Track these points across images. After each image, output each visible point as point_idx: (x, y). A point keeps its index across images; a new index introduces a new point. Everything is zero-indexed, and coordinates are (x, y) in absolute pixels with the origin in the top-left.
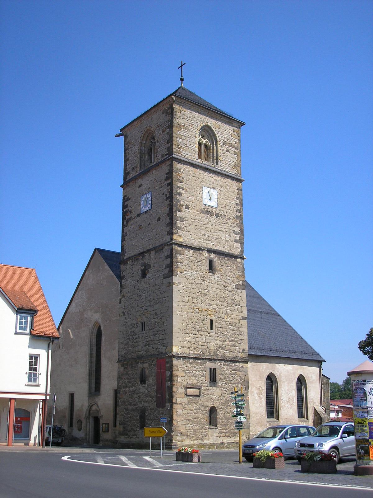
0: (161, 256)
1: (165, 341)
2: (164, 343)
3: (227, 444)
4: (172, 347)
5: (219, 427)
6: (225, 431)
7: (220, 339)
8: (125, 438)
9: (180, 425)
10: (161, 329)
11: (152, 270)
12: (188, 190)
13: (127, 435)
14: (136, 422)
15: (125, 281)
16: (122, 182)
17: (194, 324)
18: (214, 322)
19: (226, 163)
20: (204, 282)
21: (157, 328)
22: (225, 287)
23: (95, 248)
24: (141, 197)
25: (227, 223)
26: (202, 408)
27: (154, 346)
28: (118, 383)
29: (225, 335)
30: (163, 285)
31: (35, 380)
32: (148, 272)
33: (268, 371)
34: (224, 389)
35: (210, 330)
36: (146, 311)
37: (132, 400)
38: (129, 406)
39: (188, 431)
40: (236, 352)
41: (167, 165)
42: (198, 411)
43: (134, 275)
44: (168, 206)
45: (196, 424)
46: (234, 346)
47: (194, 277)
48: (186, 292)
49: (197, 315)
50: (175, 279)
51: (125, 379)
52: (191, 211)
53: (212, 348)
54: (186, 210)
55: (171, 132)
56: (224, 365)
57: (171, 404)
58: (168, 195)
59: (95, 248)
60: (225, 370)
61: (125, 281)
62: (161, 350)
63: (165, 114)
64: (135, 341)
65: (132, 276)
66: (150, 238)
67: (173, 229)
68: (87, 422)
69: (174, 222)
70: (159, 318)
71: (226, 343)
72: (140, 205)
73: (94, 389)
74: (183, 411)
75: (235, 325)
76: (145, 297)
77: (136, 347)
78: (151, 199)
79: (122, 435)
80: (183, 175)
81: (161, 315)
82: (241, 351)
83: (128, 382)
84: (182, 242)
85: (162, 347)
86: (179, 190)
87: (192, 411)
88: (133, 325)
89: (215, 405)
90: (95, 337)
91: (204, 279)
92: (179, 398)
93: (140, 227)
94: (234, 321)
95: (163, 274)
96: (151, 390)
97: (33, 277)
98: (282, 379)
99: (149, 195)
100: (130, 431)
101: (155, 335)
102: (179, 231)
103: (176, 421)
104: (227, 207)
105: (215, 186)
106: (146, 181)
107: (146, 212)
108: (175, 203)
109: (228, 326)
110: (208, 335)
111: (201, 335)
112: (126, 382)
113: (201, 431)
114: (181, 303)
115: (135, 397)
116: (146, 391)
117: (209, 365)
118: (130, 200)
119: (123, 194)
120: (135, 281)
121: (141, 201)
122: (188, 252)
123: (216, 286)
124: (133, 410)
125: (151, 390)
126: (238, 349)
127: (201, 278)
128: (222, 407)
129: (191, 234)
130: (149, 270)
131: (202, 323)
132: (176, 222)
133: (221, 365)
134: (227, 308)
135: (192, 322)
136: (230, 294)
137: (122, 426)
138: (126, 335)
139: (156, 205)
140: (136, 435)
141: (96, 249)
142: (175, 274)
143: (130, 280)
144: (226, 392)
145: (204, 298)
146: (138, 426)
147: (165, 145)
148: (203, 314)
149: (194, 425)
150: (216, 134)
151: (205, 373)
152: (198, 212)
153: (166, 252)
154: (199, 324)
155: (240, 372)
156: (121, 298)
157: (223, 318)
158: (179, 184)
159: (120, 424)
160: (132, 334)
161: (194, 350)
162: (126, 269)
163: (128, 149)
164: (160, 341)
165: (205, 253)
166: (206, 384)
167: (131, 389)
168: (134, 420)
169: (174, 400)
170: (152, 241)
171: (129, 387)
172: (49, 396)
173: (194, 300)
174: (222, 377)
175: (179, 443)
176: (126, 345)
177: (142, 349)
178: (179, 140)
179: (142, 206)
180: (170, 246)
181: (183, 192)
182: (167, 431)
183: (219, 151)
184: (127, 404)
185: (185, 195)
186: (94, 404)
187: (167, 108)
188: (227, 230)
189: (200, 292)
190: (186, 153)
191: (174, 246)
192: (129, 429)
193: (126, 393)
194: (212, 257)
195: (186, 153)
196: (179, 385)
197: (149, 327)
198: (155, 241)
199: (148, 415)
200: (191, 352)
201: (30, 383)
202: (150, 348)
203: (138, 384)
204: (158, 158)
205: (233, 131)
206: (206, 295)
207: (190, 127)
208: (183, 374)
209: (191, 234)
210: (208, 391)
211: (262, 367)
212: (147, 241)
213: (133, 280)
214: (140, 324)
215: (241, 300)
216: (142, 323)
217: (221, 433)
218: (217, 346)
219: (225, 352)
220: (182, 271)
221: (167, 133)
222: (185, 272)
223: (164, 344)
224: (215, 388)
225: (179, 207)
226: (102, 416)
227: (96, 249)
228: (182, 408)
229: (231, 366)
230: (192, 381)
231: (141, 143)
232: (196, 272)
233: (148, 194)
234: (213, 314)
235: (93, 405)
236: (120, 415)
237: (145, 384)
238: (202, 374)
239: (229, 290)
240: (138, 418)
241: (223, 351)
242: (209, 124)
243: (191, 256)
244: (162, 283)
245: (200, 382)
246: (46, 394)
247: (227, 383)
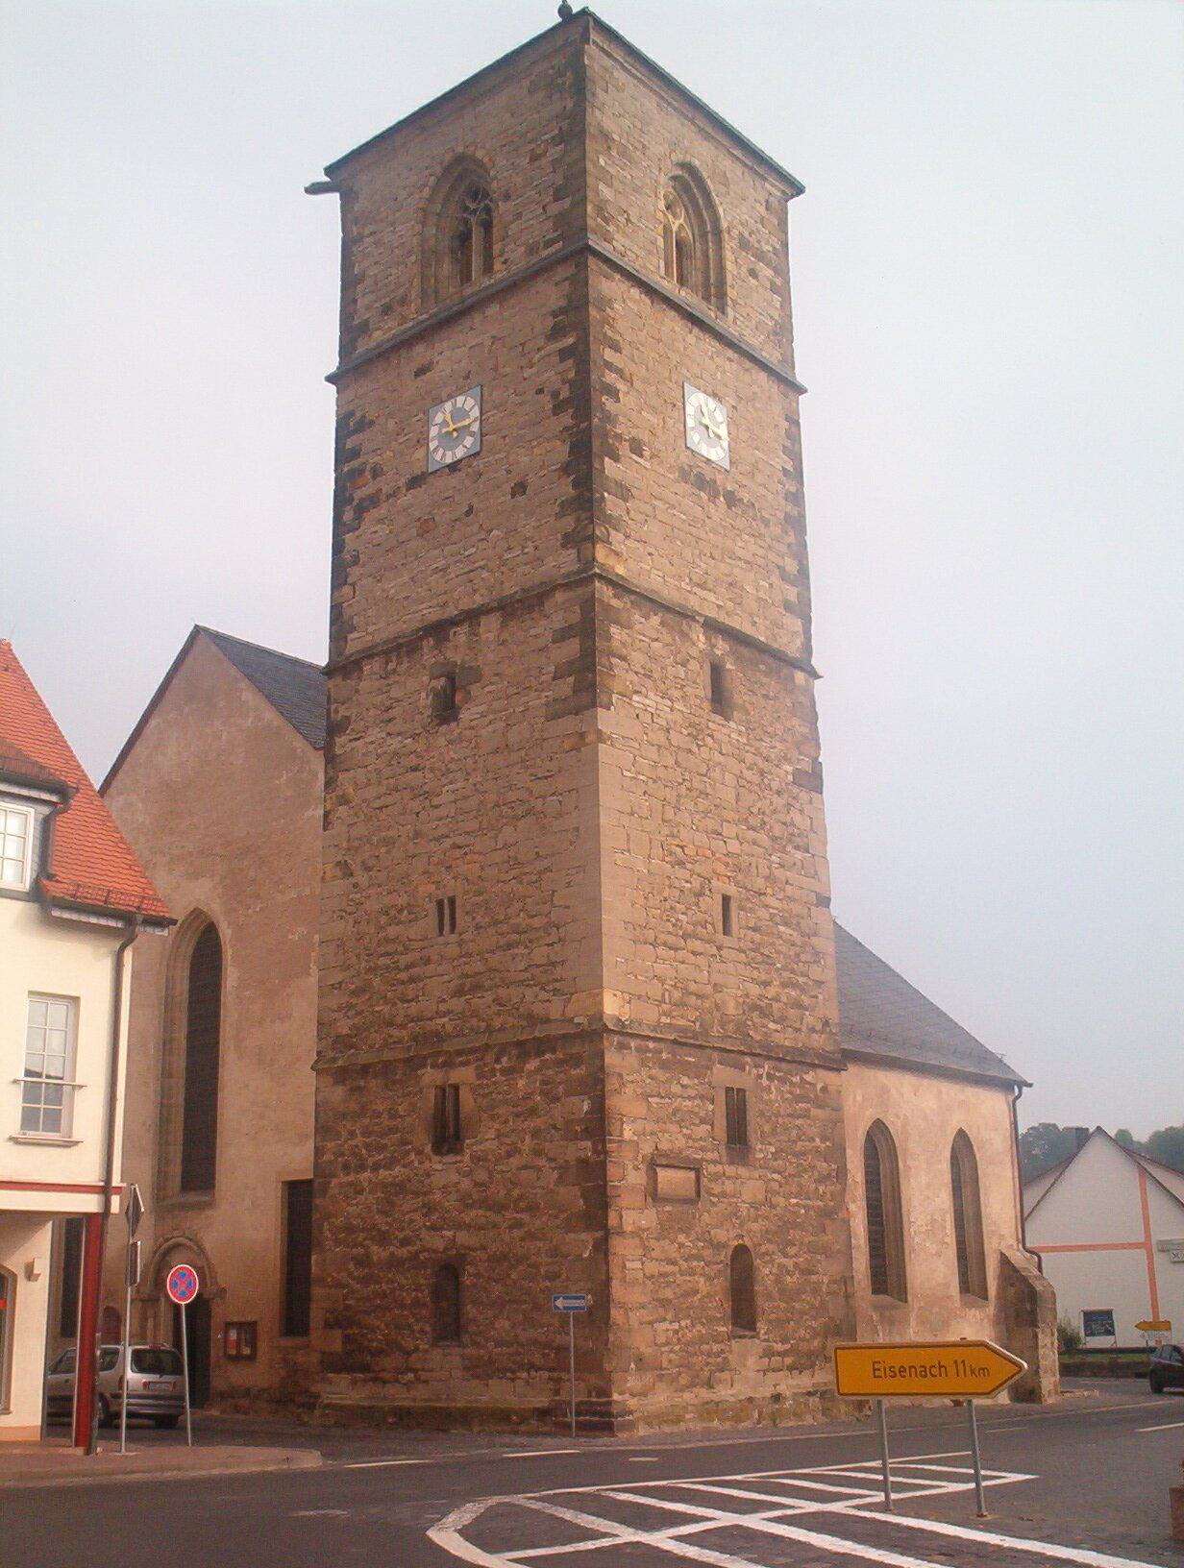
0: (533, 632)
1: (558, 972)
2: (556, 980)
3: (793, 1399)
4: (602, 992)
5: (762, 1332)
6: (779, 1347)
7: (755, 974)
8: (354, 1382)
9: (636, 1327)
10: (537, 922)
11: (486, 689)
12: (637, 384)
13: (365, 1368)
14: (414, 1315)
15: (351, 741)
16: (332, 364)
17: (672, 908)
18: (733, 906)
19: (748, 315)
20: (698, 745)
21: (519, 920)
22: (762, 773)
23: (196, 626)
24: (426, 413)
25: (760, 536)
26: (707, 1253)
27: (502, 992)
28: (318, 1152)
29: (768, 961)
30: (545, 744)
31: (54, 1121)
32: (468, 698)
33: (867, 1113)
34: (774, 1175)
35: (720, 936)
36: (458, 853)
37: (389, 1220)
38: (374, 1249)
39: (663, 1349)
40: (804, 1028)
41: (557, 278)
42: (695, 1263)
43: (391, 713)
44: (566, 435)
45: (689, 1322)
46: (799, 1005)
47: (664, 724)
48: (641, 777)
49: (679, 872)
50: (607, 720)
51: (352, 1134)
52: (648, 465)
53: (731, 1009)
54: (634, 457)
55: (575, 155)
56: (770, 1077)
57: (599, 1234)
58: (565, 394)
59: (196, 626)
60: (773, 1097)
61: (351, 741)
62: (539, 1009)
63: (540, 96)
64: (404, 976)
65: (386, 716)
66: (476, 565)
67: (592, 522)
68: (144, 1319)
69: (598, 495)
70: (526, 879)
71: (772, 992)
72: (423, 440)
73: (178, 1179)
74: (643, 1264)
75: (799, 923)
76: (452, 797)
77: (408, 1001)
78: (478, 414)
79: (338, 1371)
80: (620, 325)
81: (541, 865)
82: (819, 1027)
83: (367, 1146)
84: (622, 578)
85: (543, 995)
86: (610, 378)
87: (672, 1263)
88: (393, 912)
89: (748, 1242)
90: (187, 973)
91: (697, 733)
92: (632, 1215)
93: (426, 527)
94: (797, 908)
95: (544, 700)
96: (491, 1176)
97: (6, 670)
98: (911, 1145)
99: (468, 403)
100: (380, 1352)
101: (510, 946)
102: (613, 532)
103: (623, 1306)
104: (759, 478)
105: (721, 390)
106: (449, 354)
107: (454, 467)
108: (596, 420)
109: (777, 924)
110: (715, 956)
111: (694, 953)
112: (357, 1146)
113: (705, 1347)
114: (625, 820)
115: (406, 1207)
116: (466, 1184)
117: (723, 1075)
118: (376, 428)
119: (338, 406)
120: (400, 738)
121: (427, 424)
122: (643, 620)
123: (732, 763)
124: (395, 1263)
125: (491, 1176)
126: (809, 1019)
127: (686, 728)
128: (771, 1247)
129: (650, 554)
130: (475, 689)
131: (697, 905)
132: (603, 496)
133: (760, 1076)
134: (770, 855)
135: (666, 900)
136: (779, 802)
137: (337, 1334)
138: (358, 956)
139: (504, 437)
140: (414, 1371)
141: (197, 631)
142: (604, 698)
143: (375, 734)
144: (781, 1186)
145: (701, 807)
146: (426, 1333)
147: (544, 208)
148: (698, 868)
149: (683, 1323)
150: (717, 202)
151: (711, 1107)
152: (671, 476)
153: (560, 612)
154: (688, 909)
155: (819, 1111)
156: (328, 807)
157: (760, 894)
158: (609, 355)
159: (328, 1325)
160: (390, 948)
161: (674, 1014)
162: (357, 691)
163: (360, 238)
164: (536, 971)
165: (700, 637)
166: (716, 1153)
167: (383, 1173)
168: (402, 1306)
169: (612, 1221)
170: (485, 574)
171: (376, 1168)
172: (118, 1197)
173: (670, 814)
174: (767, 1128)
175: (632, 1403)
176: (355, 993)
177: (443, 1007)
178: (606, 192)
179: (432, 445)
180: (579, 591)
181: (622, 387)
182: (1026, 1365)
183: (729, 266)
184: (365, 1239)
185: (628, 400)
186: (182, 1240)
187: (553, 68)
188: (761, 561)
189: (687, 784)
190: (628, 243)
191: (597, 584)
192: (375, 1344)
193: (360, 1192)
194: (719, 653)
195: (628, 243)
196: (627, 1154)
197: (474, 918)
198: (502, 573)
199: (474, 1285)
200: (665, 1020)
201: (31, 1134)
202: (483, 1001)
203: (419, 1152)
204: (513, 258)
205: (767, 209)
206: (703, 796)
207: (638, 153)
208: (640, 1109)
209: (650, 554)
210: (723, 1183)
211: (851, 1097)
212: (457, 576)
213: (389, 734)
214: (432, 907)
215: (812, 829)
216: (440, 903)
217: (769, 1353)
218: (748, 1000)
219: (772, 1026)
220: (628, 694)
221: (554, 162)
222: (636, 698)
223: (557, 985)
224: (742, 1171)
225: (611, 441)
226: (223, 1291)
227: (197, 631)
228: (640, 1252)
229: (791, 1082)
230: (673, 1140)
231: (424, 210)
232: (670, 703)
233: (460, 399)
234: (729, 874)
235: (178, 1245)
236: (330, 1287)
237: (459, 1151)
238: (702, 1114)
239: (775, 785)
240: (425, 1296)
241: (765, 1021)
242: (696, 163)
243: (655, 637)
244: (537, 735)
245: (696, 1145)
246: (105, 1190)
247: (782, 1151)
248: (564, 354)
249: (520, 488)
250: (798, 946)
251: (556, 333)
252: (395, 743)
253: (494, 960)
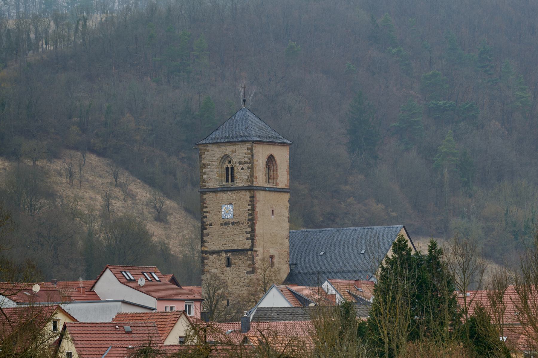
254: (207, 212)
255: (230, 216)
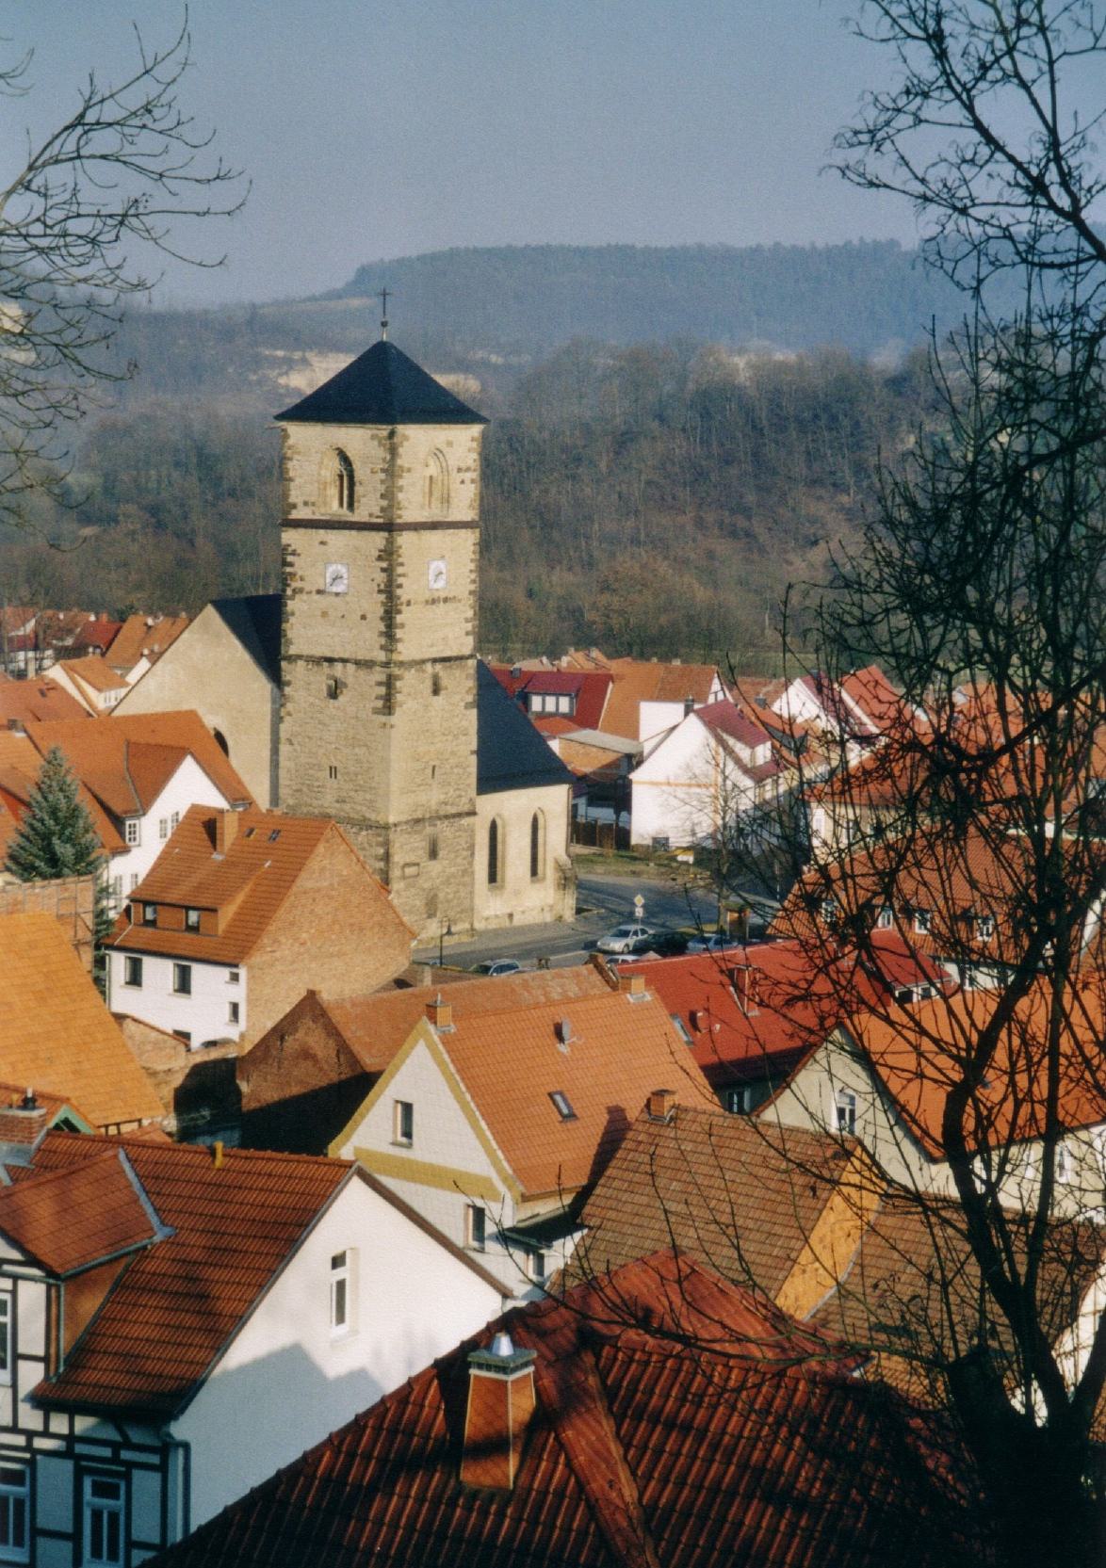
202: (347, 807)
248: (383, 570)
249: (363, 617)
250: (1033, 1109)
251: (379, 558)
252: (311, 699)
253: (352, 794)
254: (404, 575)
255: (440, 584)
